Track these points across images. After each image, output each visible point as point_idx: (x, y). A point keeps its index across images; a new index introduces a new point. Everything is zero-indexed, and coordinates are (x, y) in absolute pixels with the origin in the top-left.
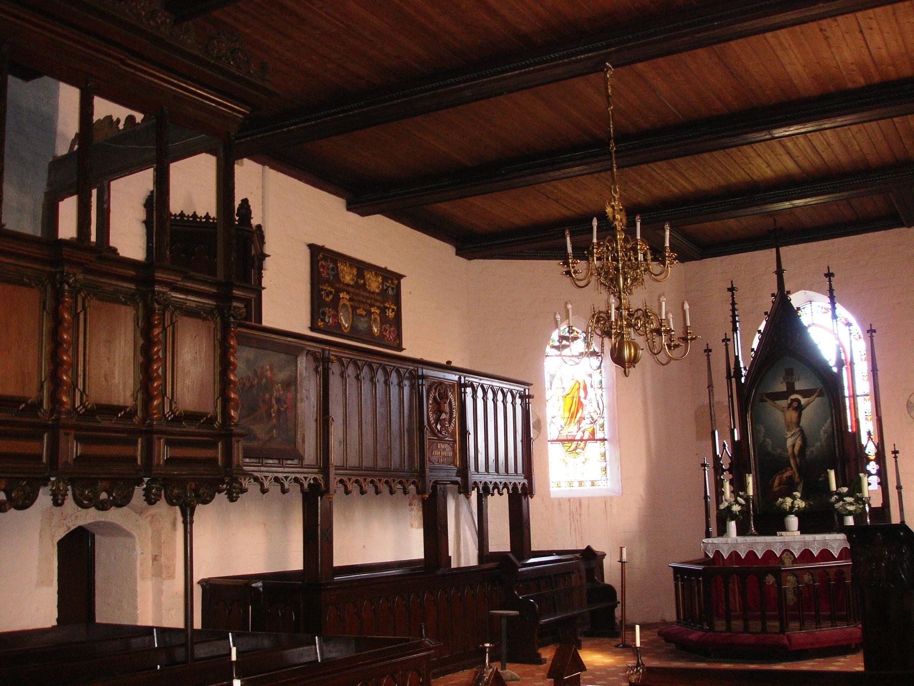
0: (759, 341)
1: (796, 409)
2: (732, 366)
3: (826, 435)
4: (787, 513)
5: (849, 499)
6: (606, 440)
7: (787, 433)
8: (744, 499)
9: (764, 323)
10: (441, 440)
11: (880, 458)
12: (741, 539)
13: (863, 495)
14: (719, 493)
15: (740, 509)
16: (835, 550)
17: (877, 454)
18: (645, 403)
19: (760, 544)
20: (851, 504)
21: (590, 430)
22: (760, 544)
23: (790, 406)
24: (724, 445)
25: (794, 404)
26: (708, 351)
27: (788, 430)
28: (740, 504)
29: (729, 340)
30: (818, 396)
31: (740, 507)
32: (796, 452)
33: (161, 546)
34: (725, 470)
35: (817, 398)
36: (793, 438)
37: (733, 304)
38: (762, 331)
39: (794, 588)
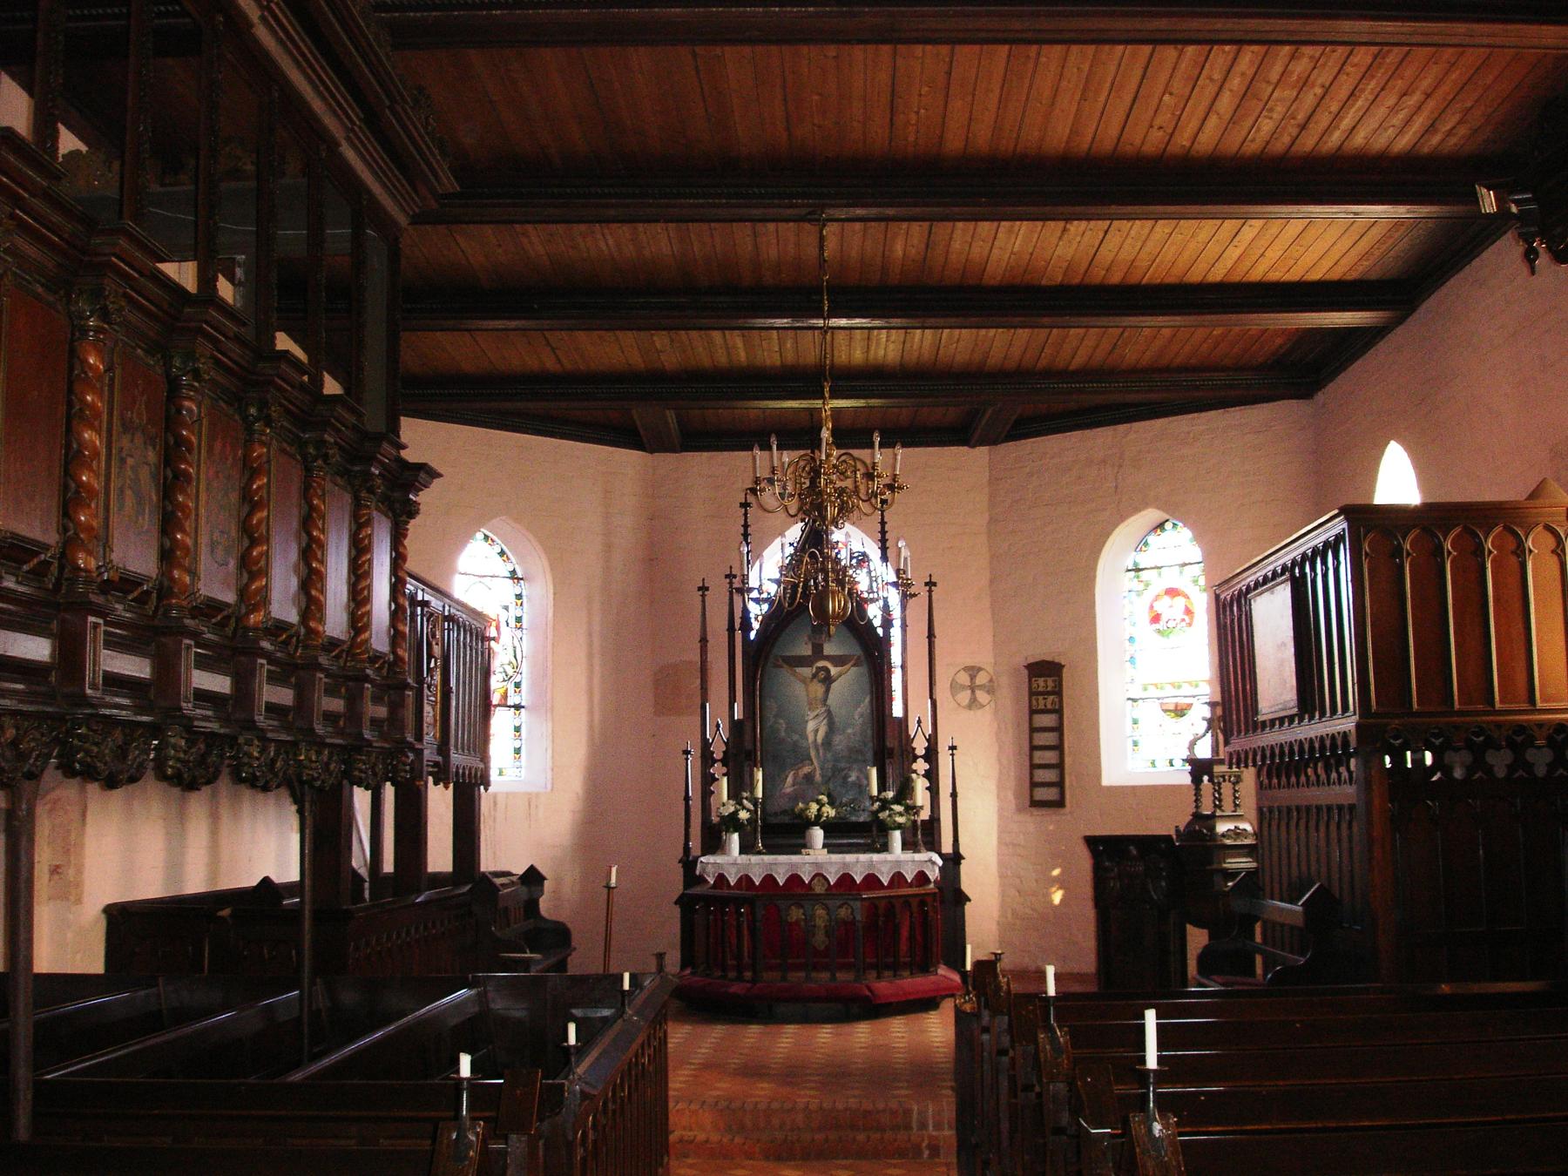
4: (810, 824)
5: (898, 808)
6: (523, 707)
11: (931, 755)
12: (909, 856)
13: (915, 802)
14: (707, 794)
16: (885, 875)
18: (590, 656)
19: (781, 865)
20: (901, 814)
21: (502, 691)
22: (781, 865)
23: (814, 676)
24: (718, 726)
26: (703, 589)
27: (810, 709)
28: (748, 810)
30: (854, 665)
32: (819, 740)
33: (68, 850)
34: (716, 761)
36: (817, 721)
37: (746, 526)
39: (825, 926)
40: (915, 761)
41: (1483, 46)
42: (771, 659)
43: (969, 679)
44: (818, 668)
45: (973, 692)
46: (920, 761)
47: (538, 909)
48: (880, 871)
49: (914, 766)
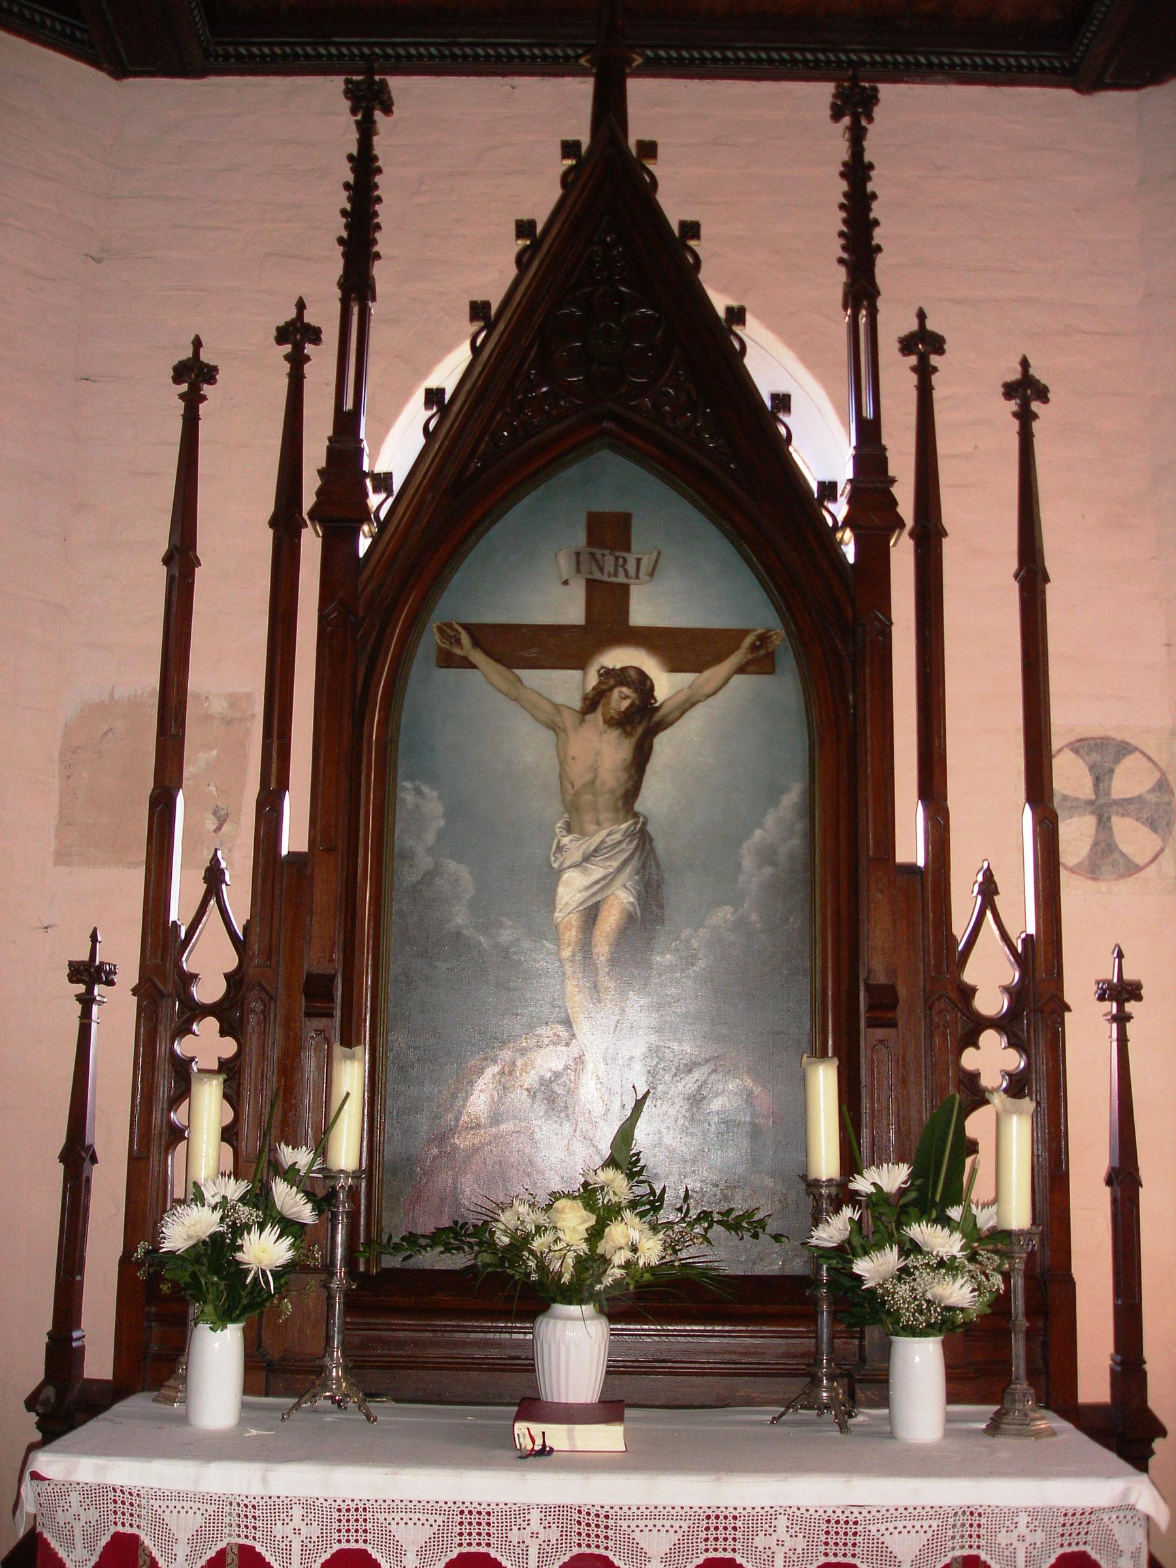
0: (421, 441)
1: (623, 722)
2: (315, 455)
3: (768, 870)
7: (565, 840)
8: (310, 1196)
9: (461, 356)
10: (569, 1120)
15: (290, 1254)
17: (1016, 994)
23: (592, 702)
25: (616, 693)
27: (569, 829)
28: (288, 1226)
29: (314, 335)
30: (741, 670)
31: (287, 1241)
35: (737, 679)
36: (597, 872)
38: (397, 484)
40: (971, 1040)
41: (273, 887)
42: (430, 640)
43: (1088, 781)
44: (607, 674)
45: (1103, 823)
46: (991, 1039)
47: (848, 513)
48: (161, 1527)
49: (970, 1059)
